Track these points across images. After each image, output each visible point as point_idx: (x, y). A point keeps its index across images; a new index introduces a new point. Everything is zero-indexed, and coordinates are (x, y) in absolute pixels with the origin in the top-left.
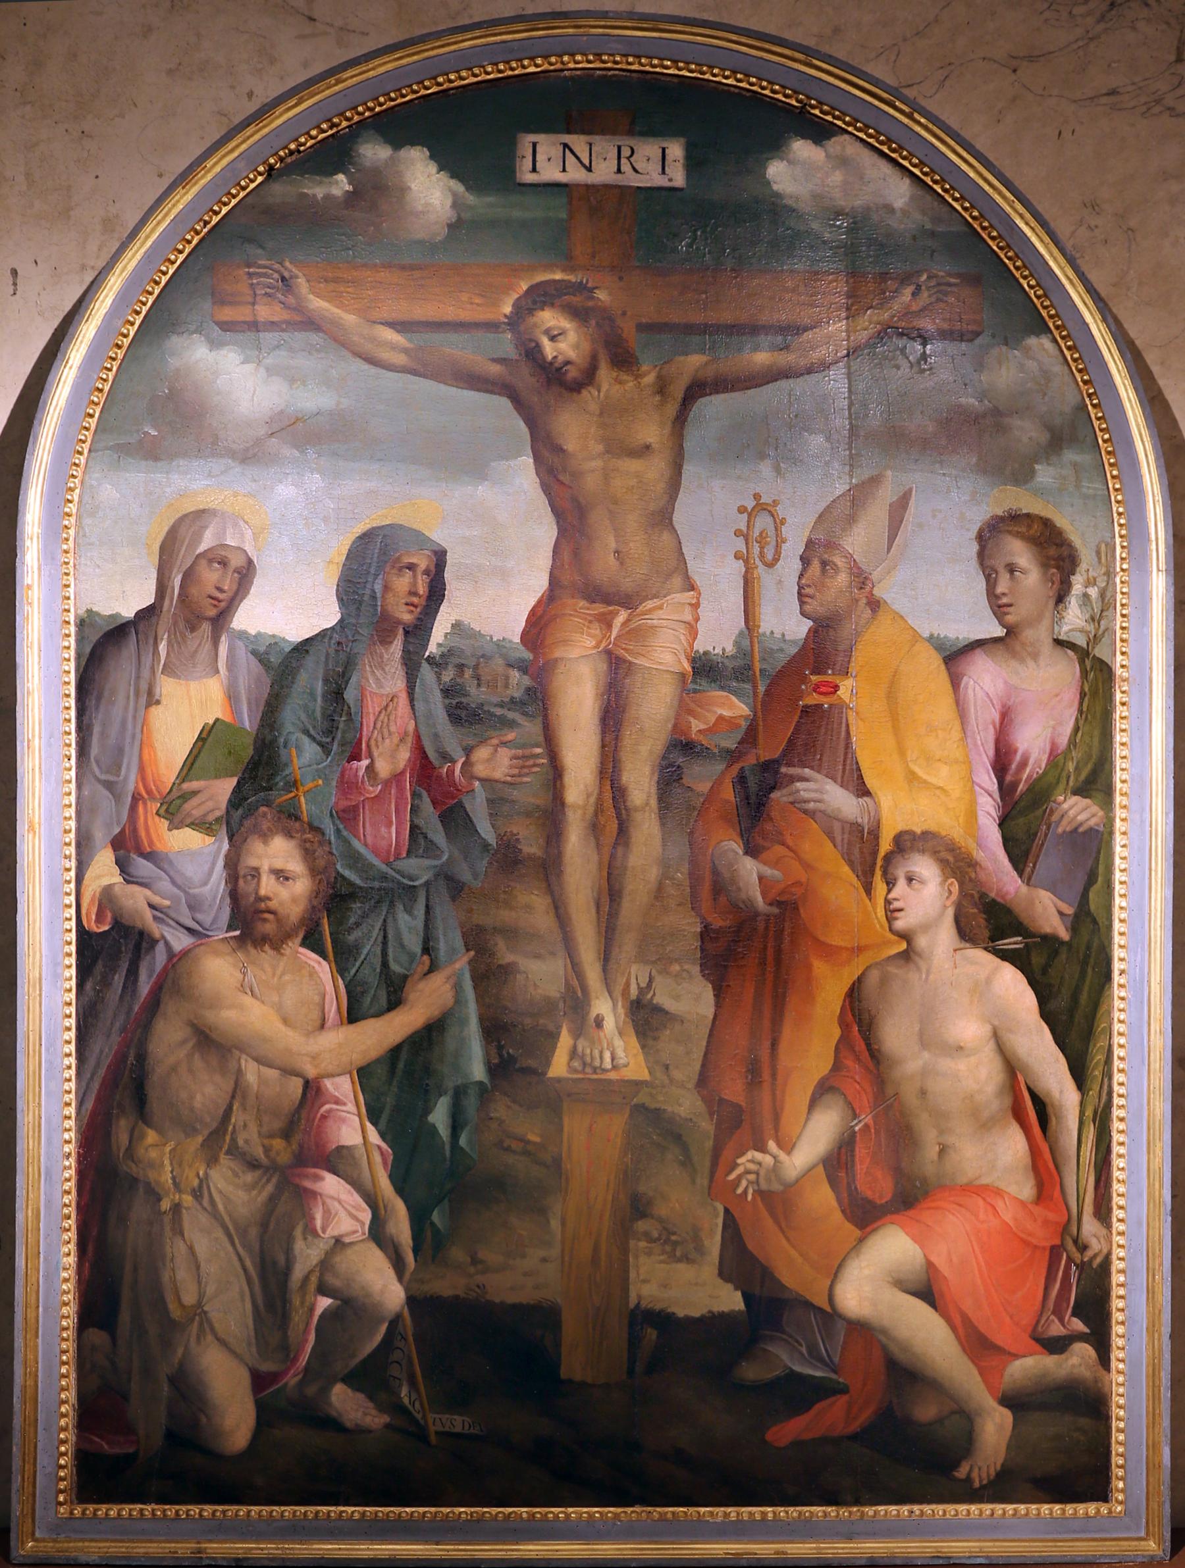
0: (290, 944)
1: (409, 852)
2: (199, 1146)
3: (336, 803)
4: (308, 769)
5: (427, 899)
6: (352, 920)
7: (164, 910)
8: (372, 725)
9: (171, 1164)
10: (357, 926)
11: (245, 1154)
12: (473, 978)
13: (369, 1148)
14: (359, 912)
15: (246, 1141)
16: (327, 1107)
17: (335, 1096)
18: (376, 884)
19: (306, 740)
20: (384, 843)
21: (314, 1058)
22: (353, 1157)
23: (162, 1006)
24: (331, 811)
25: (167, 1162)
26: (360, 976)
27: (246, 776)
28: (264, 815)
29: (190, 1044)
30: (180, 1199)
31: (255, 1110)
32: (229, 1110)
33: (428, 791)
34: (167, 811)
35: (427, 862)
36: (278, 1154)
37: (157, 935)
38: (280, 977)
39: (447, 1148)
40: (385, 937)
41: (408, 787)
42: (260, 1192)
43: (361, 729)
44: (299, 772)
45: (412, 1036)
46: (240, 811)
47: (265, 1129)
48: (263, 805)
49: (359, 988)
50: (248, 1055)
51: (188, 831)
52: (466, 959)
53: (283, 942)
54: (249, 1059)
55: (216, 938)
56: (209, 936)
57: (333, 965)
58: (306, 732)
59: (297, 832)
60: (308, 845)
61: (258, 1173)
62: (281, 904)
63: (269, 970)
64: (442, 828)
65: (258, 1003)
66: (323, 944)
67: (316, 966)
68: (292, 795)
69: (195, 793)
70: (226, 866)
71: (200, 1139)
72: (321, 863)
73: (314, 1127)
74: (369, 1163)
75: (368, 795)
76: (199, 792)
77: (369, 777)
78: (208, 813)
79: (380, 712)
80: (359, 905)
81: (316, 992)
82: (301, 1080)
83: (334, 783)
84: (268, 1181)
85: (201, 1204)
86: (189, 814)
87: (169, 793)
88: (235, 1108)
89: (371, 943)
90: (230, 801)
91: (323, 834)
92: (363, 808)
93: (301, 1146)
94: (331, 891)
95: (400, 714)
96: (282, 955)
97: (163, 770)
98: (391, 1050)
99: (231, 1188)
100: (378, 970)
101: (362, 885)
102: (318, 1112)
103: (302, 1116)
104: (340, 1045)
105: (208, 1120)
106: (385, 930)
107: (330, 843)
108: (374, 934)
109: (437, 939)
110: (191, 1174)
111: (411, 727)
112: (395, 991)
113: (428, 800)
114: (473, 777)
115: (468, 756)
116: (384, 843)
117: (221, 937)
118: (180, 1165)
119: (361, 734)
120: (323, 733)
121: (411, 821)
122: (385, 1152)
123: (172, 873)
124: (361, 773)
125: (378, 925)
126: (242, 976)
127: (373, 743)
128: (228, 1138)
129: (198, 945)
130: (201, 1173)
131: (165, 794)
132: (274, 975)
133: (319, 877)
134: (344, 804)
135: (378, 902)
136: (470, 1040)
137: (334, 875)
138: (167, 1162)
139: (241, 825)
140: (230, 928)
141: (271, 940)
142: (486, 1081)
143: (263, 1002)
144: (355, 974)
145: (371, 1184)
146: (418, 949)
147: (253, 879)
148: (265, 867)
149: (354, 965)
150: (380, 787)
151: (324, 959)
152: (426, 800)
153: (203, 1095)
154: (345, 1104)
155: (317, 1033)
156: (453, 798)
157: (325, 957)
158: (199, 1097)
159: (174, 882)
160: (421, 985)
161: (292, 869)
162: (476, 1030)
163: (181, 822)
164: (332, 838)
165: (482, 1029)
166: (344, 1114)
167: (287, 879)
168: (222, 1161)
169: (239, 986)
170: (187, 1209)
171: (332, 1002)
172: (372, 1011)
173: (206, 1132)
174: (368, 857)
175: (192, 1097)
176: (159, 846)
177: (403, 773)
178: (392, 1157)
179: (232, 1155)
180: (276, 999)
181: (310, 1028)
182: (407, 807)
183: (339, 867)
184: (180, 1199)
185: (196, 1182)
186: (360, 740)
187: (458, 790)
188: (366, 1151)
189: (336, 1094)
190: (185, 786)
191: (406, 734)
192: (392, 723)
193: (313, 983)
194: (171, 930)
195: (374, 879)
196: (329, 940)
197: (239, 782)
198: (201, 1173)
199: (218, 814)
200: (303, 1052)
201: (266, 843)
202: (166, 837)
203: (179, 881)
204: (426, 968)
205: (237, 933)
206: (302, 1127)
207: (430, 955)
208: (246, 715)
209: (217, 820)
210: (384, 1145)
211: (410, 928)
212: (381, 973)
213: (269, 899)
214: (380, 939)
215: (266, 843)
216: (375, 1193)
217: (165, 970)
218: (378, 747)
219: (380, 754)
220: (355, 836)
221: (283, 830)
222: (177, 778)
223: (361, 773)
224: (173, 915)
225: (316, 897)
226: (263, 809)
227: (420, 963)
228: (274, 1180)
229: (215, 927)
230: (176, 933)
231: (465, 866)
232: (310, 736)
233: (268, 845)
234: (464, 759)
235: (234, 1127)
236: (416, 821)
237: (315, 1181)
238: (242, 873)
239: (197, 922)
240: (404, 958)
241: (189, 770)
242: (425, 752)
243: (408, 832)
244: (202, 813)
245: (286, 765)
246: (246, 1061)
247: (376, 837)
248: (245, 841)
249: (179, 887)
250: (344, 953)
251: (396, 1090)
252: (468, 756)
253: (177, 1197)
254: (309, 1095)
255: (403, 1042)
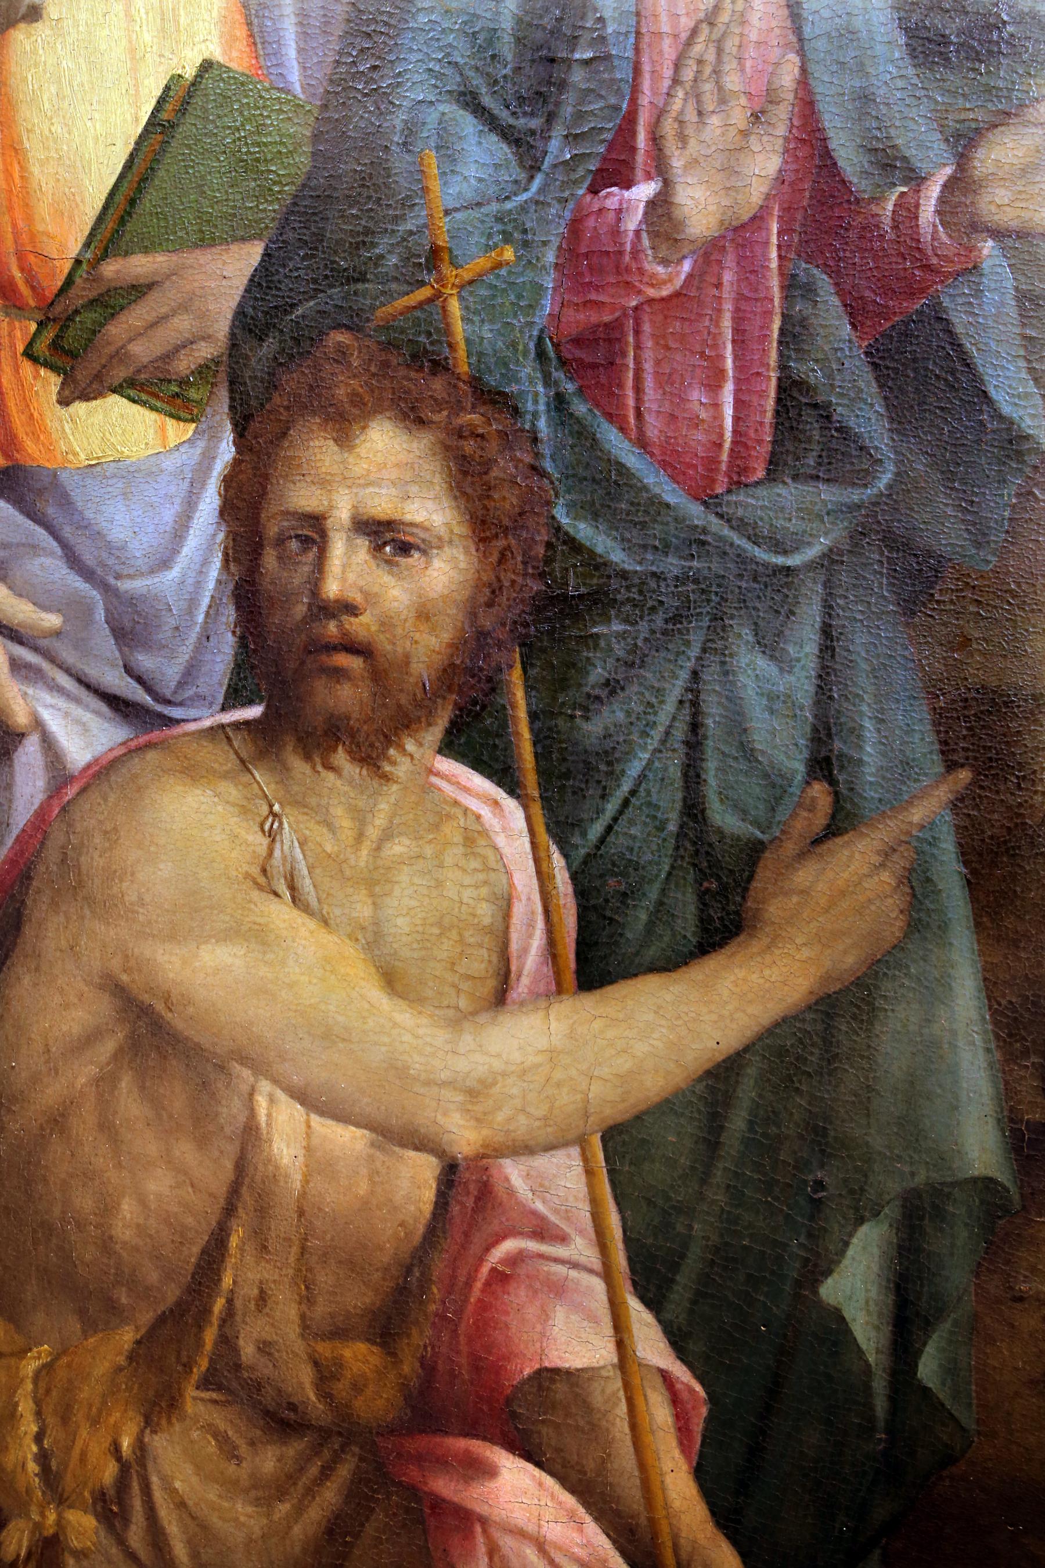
0: (410, 746)
1: (774, 465)
2: (121, 1360)
3: (555, 318)
4: (475, 214)
5: (828, 608)
6: (598, 673)
7: (43, 643)
8: (668, 72)
9: (39, 1414)
10: (613, 693)
11: (259, 1386)
12: (966, 853)
13: (636, 1381)
14: (619, 649)
15: (265, 1348)
16: (509, 1246)
17: (534, 1213)
18: (672, 565)
19: (468, 124)
20: (698, 438)
21: (473, 1094)
22: (587, 1407)
23: (28, 930)
24: (540, 340)
25: (25, 1407)
26: (618, 843)
27: (290, 235)
28: (342, 351)
29: (109, 1046)
30: (60, 1522)
31: (295, 1249)
32: (218, 1242)
33: (833, 272)
34: (55, 345)
35: (829, 495)
36: (357, 1387)
37: (21, 718)
38: (378, 849)
39: (880, 1385)
40: (695, 726)
41: (774, 264)
42: (299, 1510)
43: (635, 89)
44: (444, 223)
45: (770, 1031)
46: (270, 346)
47: (321, 1309)
48: (338, 326)
49: (612, 881)
50: (275, 1081)
51: (116, 405)
52: (943, 793)
53: (388, 742)
54: (281, 1096)
55: (192, 727)
56: (172, 722)
57: (537, 809)
58: (470, 101)
59: (438, 405)
60: (469, 446)
61: (294, 1448)
62: (386, 624)
63: (346, 823)
64: (874, 388)
65: (312, 924)
66: (508, 746)
67: (485, 812)
68: (424, 293)
69: (139, 290)
70: (228, 510)
71: (127, 1336)
72: (508, 500)
73: (470, 1309)
74: (634, 1427)
75: (652, 292)
76: (151, 286)
77: (654, 235)
78: (177, 349)
79: (694, 32)
80: (617, 627)
81: (484, 891)
82: (433, 1160)
83: (550, 257)
84: (327, 1471)
85: (121, 1541)
86: (120, 356)
87: (63, 290)
88: (234, 1241)
89: (653, 743)
90: (240, 313)
91: (516, 412)
92: (637, 332)
93: (428, 1368)
94: (536, 586)
95: (754, 36)
96: (386, 778)
97: (45, 220)
98: (708, 1073)
99: (212, 1494)
100: (672, 827)
101: (630, 565)
102: (481, 1260)
103: (435, 1275)
104: (552, 1054)
105: (153, 1277)
106: (695, 704)
107: (535, 440)
108: (663, 718)
109: (856, 732)
110: (97, 1448)
111: (788, 77)
112: (724, 891)
113: (835, 301)
114: (977, 227)
115: (963, 161)
116: (698, 438)
117: (207, 723)
118: (65, 1419)
119: (634, 101)
120: (521, 100)
121: (783, 367)
122: (685, 1396)
123: (67, 532)
124: (632, 223)
125: (676, 689)
126: (265, 841)
127: (668, 127)
128: (210, 1336)
129: (139, 749)
130: (126, 1443)
131: (50, 293)
132: (360, 837)
133: (501, 543)
134: (578, 319)
135: (676, 619)
136: (953, 1046)
137: (543, 536)
138: (25, 1407)
139: (272, 385)
140: (235, 697)
141: (353, 734)
142: (1003, 1176)
143: (325, 922)
144: (602, 840)
145: (637, 1494)
146: (797, 766)
147: (305, 550)
148: (342, 513)
149: (599, 811)
150: (687, 266)
151: (511, 792)
152: (830, 300)
153: (143, 1202)
154: (563, 1239)
155: (483, 1018)
156: (912, 294)
157: (513, 788)
158: (128, 1208)
159: (73, 560)
160: (804, 875)
161: (418, 518)
162: (974, 1015)
163: (98, 377)
164: (542, 424)
165: (994, 1013)
166: (561, 1269)
167: (405, 549)
168: (190, 1408)
169: (255, 871)
170: (81, 1555)
171: (531, 925)
172: (652, 952)
173: (146, 1317)
174: (650, 480)
175: (107, 1209)
176: (32, 452)
177: (758, 219)
178: (704, 1411)
179: (219, 1388)
180: (363, 911)
181: (463, 1003)
182: (766, 326)
183: (561, 514)
184: (60, 1522)
185: (109, 1472)
186: (631, 119)
187: (927, 268)
188: (627, 1386)
189: (539, 1206)
190: (110, 269)
191: (771, 97)
192: (730, 65)
193: (474, 864)
194: (62, 703)
195: (666, 548)
196: (526, 734)
197: (267, 255)
198: (126, 1443)
199: (205, 351)
200: (444, 1076)
201: (344, 440)
202: (52, 424)
203: (88, 558)
204: (820, 820)
205: (255, 712)
206: (433, 1307)
207: (832, 781)
208: (291, 52)
209: (204, 371)
210: (681, 1372)
211: (772, 697)
212: (681, 835)
213: (350, 609)
214: (680, 733)
215: (344, 440)
216: (652, 1522)
217: (41, 819)
218: (683, 139)
219: (693, 163)
220: (610, 417)
221: (395, 402)
222: (87, 245)
223: (632, 223)
224: (69, 656)
225: (490, 604)
226: (341, 337)
227: (800, 805)
228: (344, 1471)
229: (190, 692)
230: (78, 712)
231: (945, 504)
232: (479, 110)
233: (351, 448)
234: (948, 171)
235: (230, 1301)
236: (799, 368)
237: (468, 1480)
238: (272, 530)
239: (140, 680)
240: (752, 790)
241: (122, 221)
242: (827, 154)
243: (770, 403)
244: (158, 351)
245: (407, 204)
246: (272, 1100)
247: (673, 417)
248: (284, 434)
249: (87, 574)
250: (567, 775)
251: (721, 1197)
252: (963, 161)
253: (52, 1517)
254: (455, 1209)
255: (747, 1049)
